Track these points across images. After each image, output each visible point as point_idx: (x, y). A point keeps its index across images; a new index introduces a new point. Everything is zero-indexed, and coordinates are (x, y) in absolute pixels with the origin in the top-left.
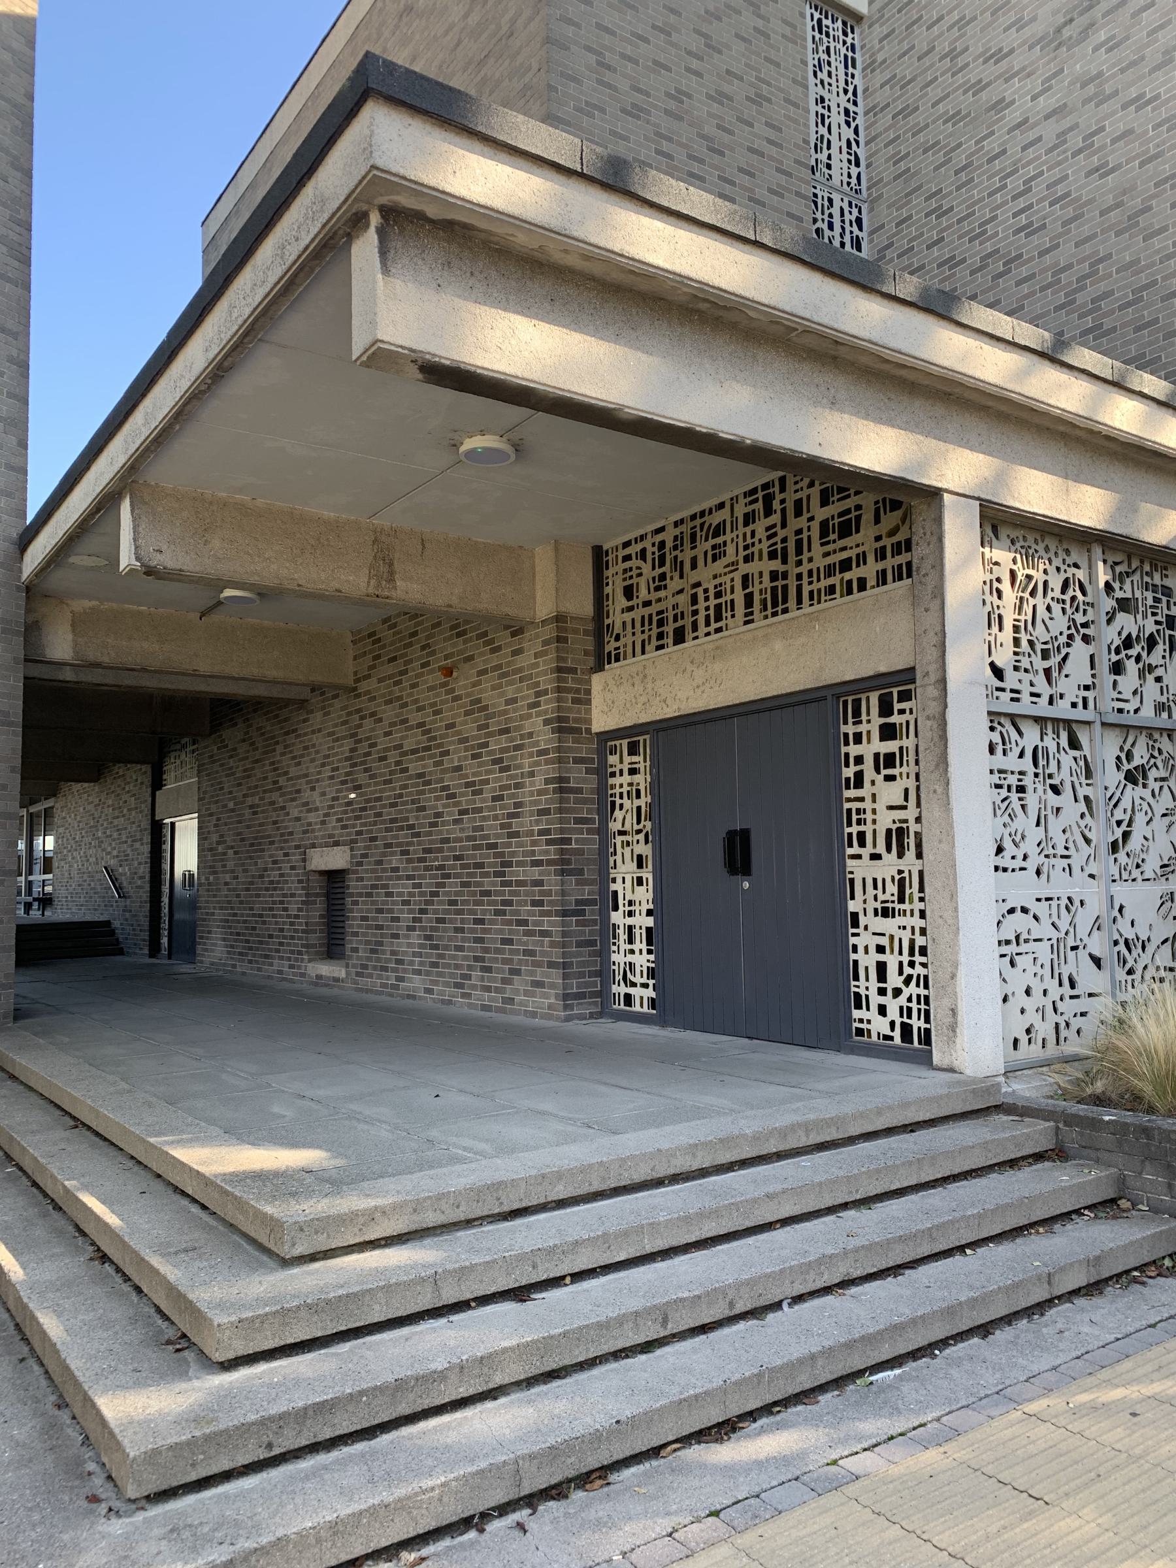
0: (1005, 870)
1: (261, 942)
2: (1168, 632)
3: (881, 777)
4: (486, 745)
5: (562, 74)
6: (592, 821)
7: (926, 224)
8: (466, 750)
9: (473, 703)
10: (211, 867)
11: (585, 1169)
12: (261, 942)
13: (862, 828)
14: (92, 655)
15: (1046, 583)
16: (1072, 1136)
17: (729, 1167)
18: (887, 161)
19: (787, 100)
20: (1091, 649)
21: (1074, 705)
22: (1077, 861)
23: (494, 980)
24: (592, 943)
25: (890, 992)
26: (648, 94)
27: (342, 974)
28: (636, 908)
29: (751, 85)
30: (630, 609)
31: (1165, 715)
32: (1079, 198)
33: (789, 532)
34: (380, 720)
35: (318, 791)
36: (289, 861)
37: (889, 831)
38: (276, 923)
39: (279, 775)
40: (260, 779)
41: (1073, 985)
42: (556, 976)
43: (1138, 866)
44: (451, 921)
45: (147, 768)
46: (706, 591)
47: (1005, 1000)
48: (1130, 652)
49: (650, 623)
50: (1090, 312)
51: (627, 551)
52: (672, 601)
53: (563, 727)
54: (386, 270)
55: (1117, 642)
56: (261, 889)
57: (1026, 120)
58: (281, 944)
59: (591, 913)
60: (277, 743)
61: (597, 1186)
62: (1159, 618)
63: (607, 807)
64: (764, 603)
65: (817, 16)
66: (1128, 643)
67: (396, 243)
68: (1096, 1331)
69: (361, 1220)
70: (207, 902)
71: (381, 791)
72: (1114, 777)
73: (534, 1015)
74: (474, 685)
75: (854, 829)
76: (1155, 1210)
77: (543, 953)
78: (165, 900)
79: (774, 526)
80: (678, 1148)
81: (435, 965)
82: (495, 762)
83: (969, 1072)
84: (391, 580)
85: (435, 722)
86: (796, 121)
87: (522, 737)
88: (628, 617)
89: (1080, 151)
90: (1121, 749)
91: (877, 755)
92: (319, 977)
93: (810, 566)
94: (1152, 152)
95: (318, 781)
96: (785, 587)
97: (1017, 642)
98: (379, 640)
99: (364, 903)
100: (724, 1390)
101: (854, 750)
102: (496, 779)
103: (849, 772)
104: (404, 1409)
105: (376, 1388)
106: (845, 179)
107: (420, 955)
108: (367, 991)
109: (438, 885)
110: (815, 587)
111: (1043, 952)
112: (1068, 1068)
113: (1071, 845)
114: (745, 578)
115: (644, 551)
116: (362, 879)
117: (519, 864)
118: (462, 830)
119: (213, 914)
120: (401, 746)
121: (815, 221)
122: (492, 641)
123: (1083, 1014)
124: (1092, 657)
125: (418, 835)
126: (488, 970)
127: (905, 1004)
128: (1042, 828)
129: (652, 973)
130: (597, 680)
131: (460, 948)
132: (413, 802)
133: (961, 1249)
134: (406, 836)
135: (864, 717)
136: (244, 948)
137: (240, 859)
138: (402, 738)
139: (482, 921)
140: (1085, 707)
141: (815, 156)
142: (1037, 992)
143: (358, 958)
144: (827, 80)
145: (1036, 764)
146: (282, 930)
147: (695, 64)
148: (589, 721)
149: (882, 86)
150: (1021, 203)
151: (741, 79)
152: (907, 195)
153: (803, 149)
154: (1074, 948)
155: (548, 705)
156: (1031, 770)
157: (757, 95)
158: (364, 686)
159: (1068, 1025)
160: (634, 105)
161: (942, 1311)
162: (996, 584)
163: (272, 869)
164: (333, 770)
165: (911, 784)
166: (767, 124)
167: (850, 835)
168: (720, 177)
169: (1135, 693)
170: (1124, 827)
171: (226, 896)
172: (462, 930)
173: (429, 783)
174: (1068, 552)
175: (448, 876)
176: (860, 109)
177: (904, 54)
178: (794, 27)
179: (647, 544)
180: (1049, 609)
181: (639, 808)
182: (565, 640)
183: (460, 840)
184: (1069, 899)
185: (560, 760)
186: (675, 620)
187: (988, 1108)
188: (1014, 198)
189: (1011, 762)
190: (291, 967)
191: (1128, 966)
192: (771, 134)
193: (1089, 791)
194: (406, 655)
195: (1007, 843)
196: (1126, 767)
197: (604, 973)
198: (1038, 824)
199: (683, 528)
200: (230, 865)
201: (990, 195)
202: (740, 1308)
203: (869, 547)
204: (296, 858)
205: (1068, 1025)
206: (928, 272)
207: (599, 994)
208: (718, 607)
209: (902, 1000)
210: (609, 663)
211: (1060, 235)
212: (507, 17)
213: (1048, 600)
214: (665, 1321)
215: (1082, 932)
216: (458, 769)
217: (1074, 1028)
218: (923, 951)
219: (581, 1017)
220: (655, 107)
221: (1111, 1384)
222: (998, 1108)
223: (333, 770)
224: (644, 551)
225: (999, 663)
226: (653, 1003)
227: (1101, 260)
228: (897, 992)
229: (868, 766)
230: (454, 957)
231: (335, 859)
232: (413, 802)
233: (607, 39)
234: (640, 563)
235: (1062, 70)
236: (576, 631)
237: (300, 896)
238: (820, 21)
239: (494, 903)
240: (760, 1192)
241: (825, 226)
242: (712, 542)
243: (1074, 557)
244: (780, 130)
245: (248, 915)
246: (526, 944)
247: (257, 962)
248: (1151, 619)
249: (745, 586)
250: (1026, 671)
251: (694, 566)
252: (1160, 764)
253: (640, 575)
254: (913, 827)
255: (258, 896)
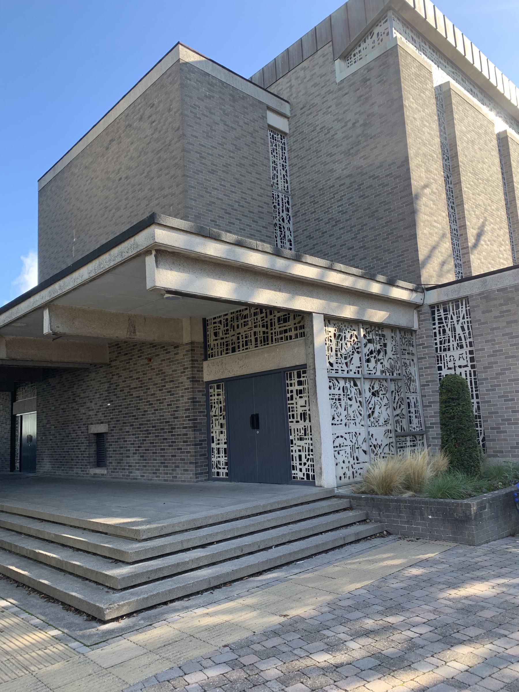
0: (335, 424)
1: (67, 462)
2: (384, 348)
3: (298, 397)
4: (165, 386)
5: (189, 161)
6: (204, 412)
7: (310, 206)
8: (157, 387)
9: (159, 371)
10: (43, 433)
11: (217, 515)
12: (67, 462)
13: (293, 413)
14: (13, 356)
15: (345, 336)
16: (354, 502)
17: (257, 514)
18: (297, 183)
19: (263, 165)
20: (360, 355)
21: (355, 373)
22: (357, 421)
23: (169, 470)
24: (205, 455)
25: (303, 464)
26: (216, 166)
27: (106, 472)
28: (220, 442)
29: (251, 160)
30: (216, 340)
31: (384, 374)
32: (357, 204)
33: (268, 319)
34: (121, 376)
35: (93, 403)
36: (80, 430)
37: (301, 413)
38: (75, 454)
39: (75, 397)
40: (66, 398)
41: (358, 460)
42: (193, 467)
43: (377, 422)
44: (151, 450)
45: (9, 394)
46: (242, 336)
47: (337, 465)
48: (372, 355)
49: (224, 345)
50: (362, 241)
51: (215, 321)
52: (231, 338)
53: (194, 380)
54: (157, 267)
55: (368, 353)
56: (67, 441)
57: (340, 177)
58: (78, 462)
59: (205, 444)
60: (75, 384)
61: (220, 520)
62: (381, 344)
63: (209, 407)
64: (261, 341)
65: (272, 134)
66: (371, 353)
67: (160, 259)
68: (355, 550)
69: (159, 529)
70: (42, 447)
71: (121, 403)
72: (368, 394)
73: (184, 481)
74: (159, 365)
75: (291, 413)
76: (376, 522)
77: (188, 460)
78: (18, 447)
79: (263, 317)
80: (242, 509)
81: (145, 466)
82: (168, 392)
83: (326, 487)
84: (134, 332)
85: (144, 377)
86: (266, 171)
87: (179, 383)
88: (216, 342)
89: (357, 190)
90: (370, 385)
91: (297, 390)
92: (95, 474)
93: (275, 331)
94: (378, 193)
95: (93, 399)
96: (267, 337)
97: (337, 355)
98: (120, 347)
99: (115, 445)
100: (258, 564)
101: (290, 388)
102: (169, 398)
103: (289, 395)
104: (179, 570)
105: (172, 565)
106: (283, 188)
107: (139, 463)
108: (116, 478)
109: (146, 437)
110: (277, 337)
111: (348, 449)
112: (356, 485)
113: (355, 416)
114: (255, 333)
115: (221, 321)
116: (113, 436)
117: (178, 428)
118: (155, 416)
119: (44, 452)
120: (130, 386)
121: (273, 203)
122: (167, 350)
123: (361, 469)
124: (360, 358)
125: (137, 419)
126: (167, 467)
127: (307, 467)
128: (346, 411)
129: (226, 464)
130: (205, 364)
131: (155, 460)
132: (135, 407)
133: (321, 533)
134: (132, 419)
135: (293, 378)
136: (60, 465)
137: (57, 430)
138: (130, 383)
139: (164, 449)
140: (358, 373)
141: (272, 181)
142: (346, 462)
143: (113, 466)
144: (276, 155)
145: (344, 392)
146: (78, 457)
147: (232, 155)
148: (202, 378)
149: (294, 158)
150: (340, 203)
151: (247, 158)
152: (304, 195)
153: (268, 180)
154: (358, 448)
155: (188, 373)
156: (342, 393)
157: (253, 163)
158: (113, 364)
159: (356, 472)
160: (212, 170)
161: (314, 546)
162: (330, 338)
163: (73, 433)
164: (100, 395)
165: (307, 399)
166: (257, 173)
167: (290, 415)
168: (241, 192)
169: (374, 368)
170: (372, 410)
171: (51, 445)
172: (156, 453)
173: (142, 399)
174: (351, 326)
175: (150, 433)
176: (287, 164)
177: (301, 148)
178: (264, 140)
179: (222, 319)
180: (346, 344)
181: (221, 407)
182: (194, 350)
183: (154, 420)
184: (356, 433)
185: (193, 392)
186: (232, 345)
187: (330, 496)
188: (338, 201)
189: (336, 391)
190: (82, 471)
191: (375, 453)
192: (258, 176)
193: (360, 399)
194: (132, 353)
195: (336, 416)
196: (372, 391)
197: (210, 465)
198: (345, 410)
199: (234, 315)
200: (53, 432)
201: (330, 199)
202: (261, 548)
203: (292, 326)
204: (83, 428)
205: (356, 472)
206: (311, 222)
207: (208, 473)
208: (246, 341)
209: (306, 466)
210: (209, 357)
211: (352, 215)
212: (168, 139)
213: (346, 341)
214: (242, 550)
215: (360, 442)
216: (154, 394)
217: (358, 473)
218: (312, 451)
219: (202, 481)
220: (220, 170)
221: (356, 559)
222: (334, 497)
223: (100, 395)
224: (221, 321)
225: (331, 362)
226: (227, 474)
227: (364, 225)
228: (305, 464)
229: (294, 393)
230: (153, 463)
231: (102, 428)
232: (135, 407)
233: (203, 149)
234: (219, 325)
235: (350, 163)
236: (198, 347)
237: (86, 443)
238: (273, 136)
239: (169, 442)
240: (265, 520)
241: (277, 205)
242: (244, 320)
243: (354, 328)
244: (260, 174)
245: (62, 452)
246: (181, 456)
247: (66, 470)
248: (379, 345)
249: (255, 335)
250: (340, 363)
251: (238, 327)
252: (383, 390)
253: (219, 329)
254: (308, 412)
255: (66, 444)
